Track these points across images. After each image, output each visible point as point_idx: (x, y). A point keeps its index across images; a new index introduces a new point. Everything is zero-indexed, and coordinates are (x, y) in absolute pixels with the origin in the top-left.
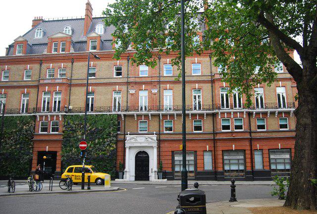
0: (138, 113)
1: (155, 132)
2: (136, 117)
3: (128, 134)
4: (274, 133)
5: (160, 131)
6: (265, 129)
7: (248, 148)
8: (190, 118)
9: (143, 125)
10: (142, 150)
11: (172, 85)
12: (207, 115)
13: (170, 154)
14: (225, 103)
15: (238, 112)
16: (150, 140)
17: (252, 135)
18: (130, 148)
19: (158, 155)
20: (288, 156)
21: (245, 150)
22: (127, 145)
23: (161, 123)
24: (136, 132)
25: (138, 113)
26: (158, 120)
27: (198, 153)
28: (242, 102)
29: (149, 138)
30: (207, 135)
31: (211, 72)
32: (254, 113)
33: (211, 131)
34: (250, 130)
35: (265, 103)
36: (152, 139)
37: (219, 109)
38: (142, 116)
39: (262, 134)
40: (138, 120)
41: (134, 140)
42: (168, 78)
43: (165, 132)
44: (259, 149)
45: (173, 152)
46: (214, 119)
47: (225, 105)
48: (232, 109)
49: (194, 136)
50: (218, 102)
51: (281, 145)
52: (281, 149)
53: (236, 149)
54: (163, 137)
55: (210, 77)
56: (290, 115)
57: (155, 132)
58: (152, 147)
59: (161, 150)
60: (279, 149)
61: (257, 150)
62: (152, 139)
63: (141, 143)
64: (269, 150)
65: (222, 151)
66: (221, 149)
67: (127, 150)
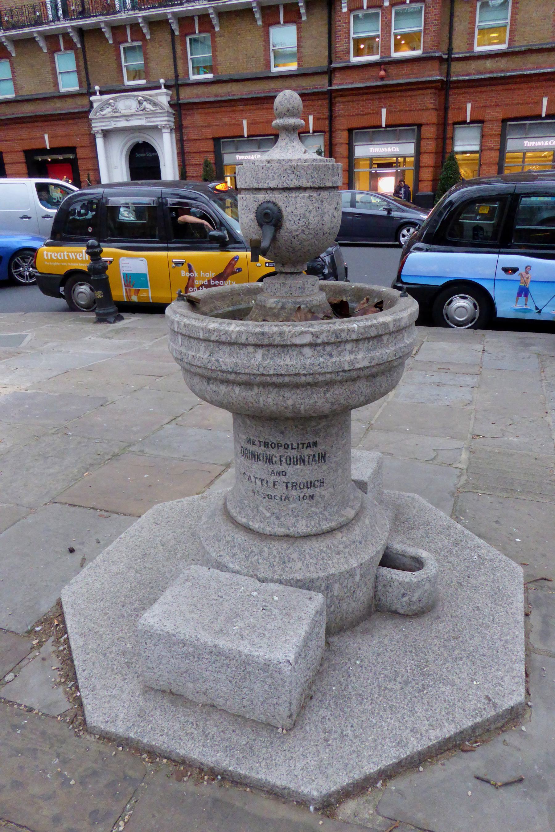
0: (113, 18)
1: (162, 81)
2: (258, 16)
3: (94, 94)
4: (533, 58)
5: (177, 76)
6: (128, 80)
7: (431, 117)
8: (260, 23)
9: (136, 62)
10: (140, 138)
13: (210, 145)
16: (149, 107)
18: (106, 134)
19: (178, 153)
20: (409, 148)
21: (420, 126)
22: (97, 126)
23: (179, 48)
24: (115, 85)
25: (113, 18)
26: (168, 37)
29: (146, 100)
30: (248, 84)
34: (450, 50)
36: (155, 104)
38: (124, 27)
40: (117, 43)
41: (109, 110)
43: (194, 78)
44: (472, 122)
45: (216, 140)
53: (475, 118)
54: (187, 96)
57: (162, 81)
58: (155, 129)
59: (185, 137)
60: (539, 117)
62: (155, 104)
63: (127, 117)
64: (504, 121)
65: (350, 131)
66: (346, 127)
67: (100, 142)
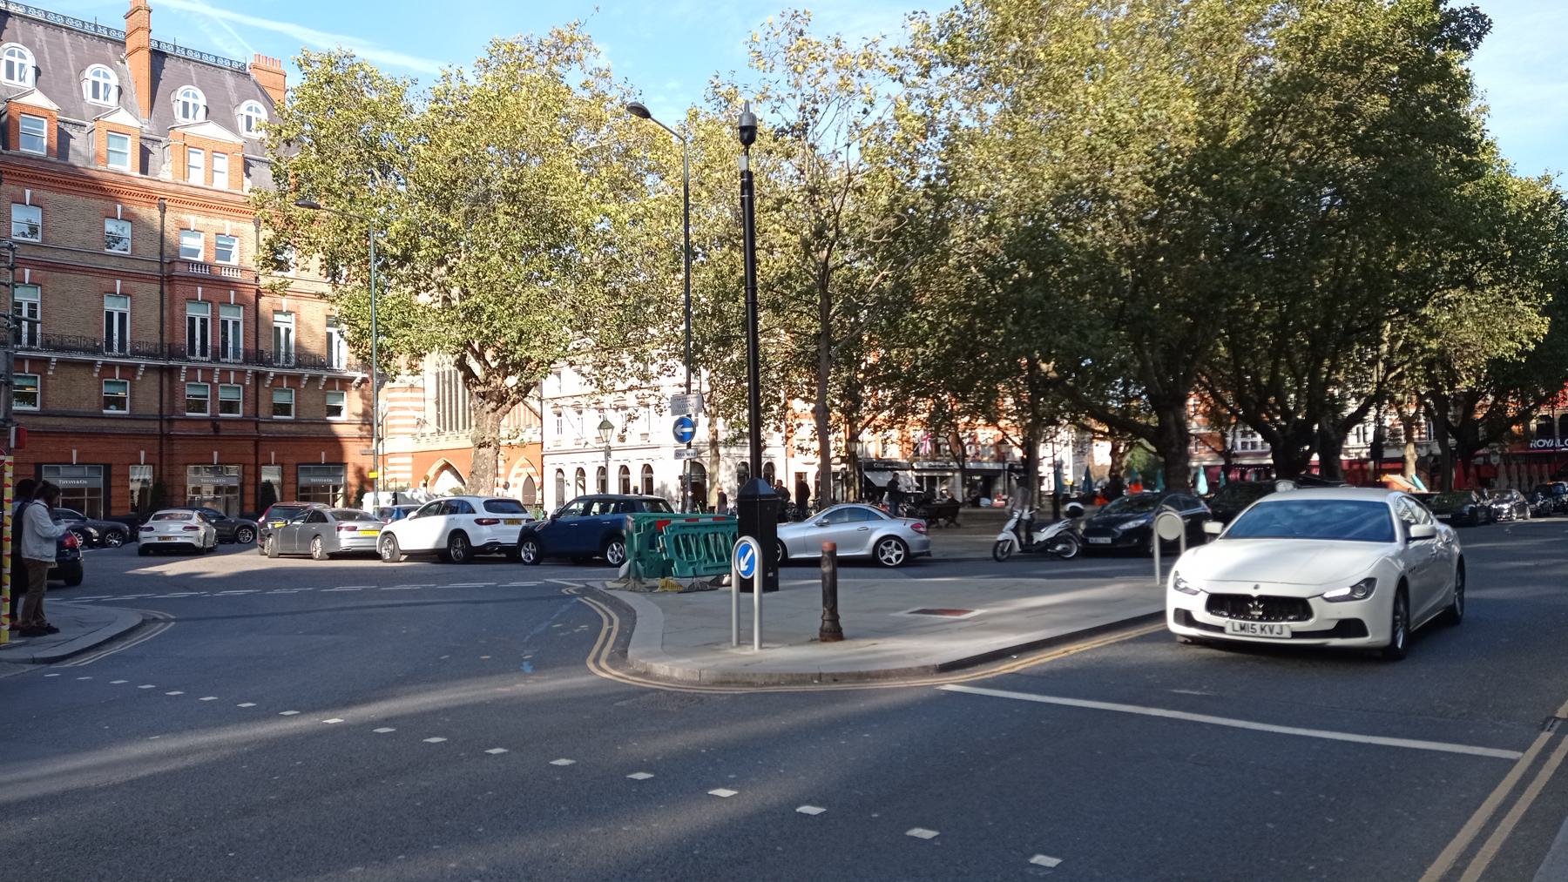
8: (96, 375)
11: (40, 274)
12: (148, 368)
14: (198, 343)
15: (232, 370)
17: (262, 427)
27: (115, 470)
28: (209, 344)
31: (161, 253)
32: (272, 375)
33: (154, 409)
34: (257, 415)
35: (131, 342)
37: (183, 357)
39: (284, 427)
42: (29, 248)
46: (260, 383)
47: (198, 348)
48: (218, 361)
49: (105, 423)
50: (179, 341)
51: (219, 455)
52: (326, 464)
55: (157, 267)
56: (135, 374)
60: (320, 464)
61: (72, 463)
64: (297, 465)
